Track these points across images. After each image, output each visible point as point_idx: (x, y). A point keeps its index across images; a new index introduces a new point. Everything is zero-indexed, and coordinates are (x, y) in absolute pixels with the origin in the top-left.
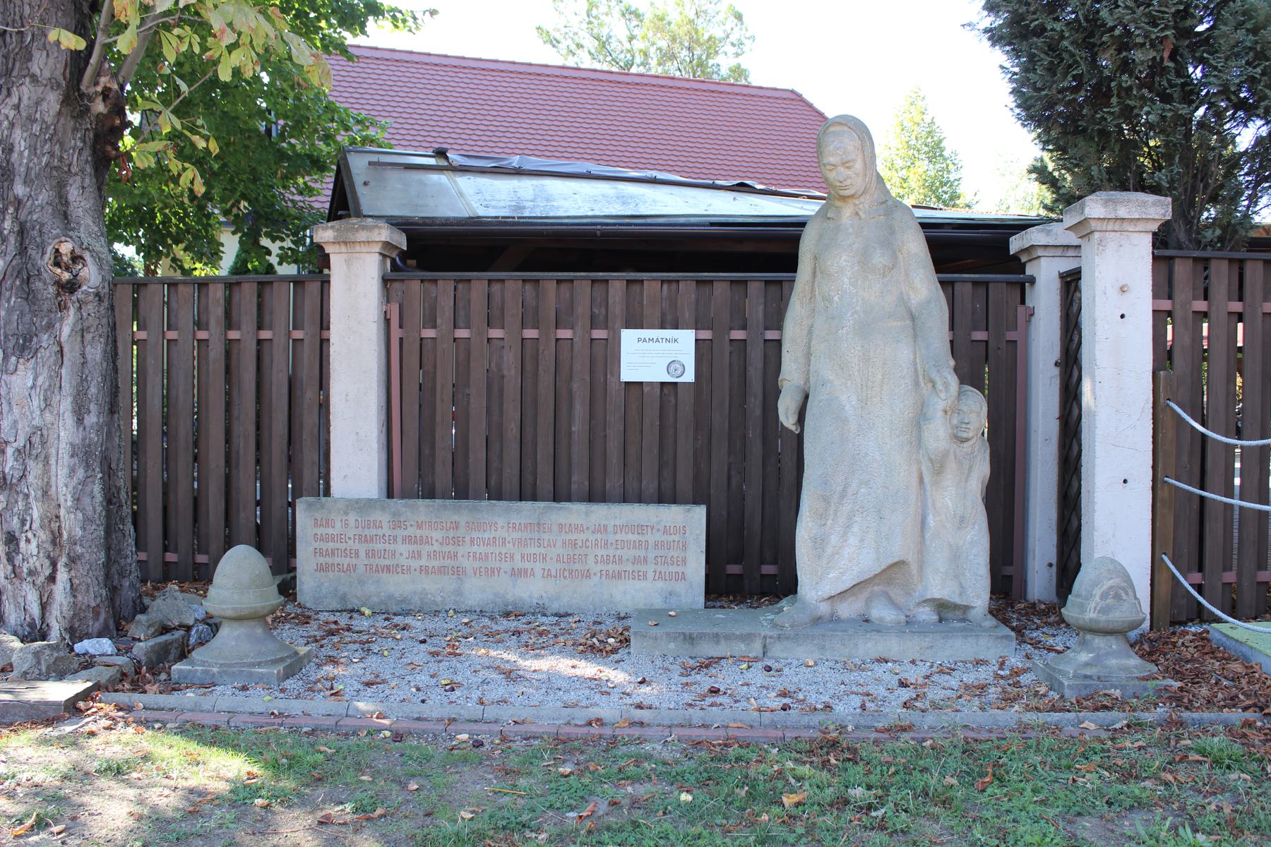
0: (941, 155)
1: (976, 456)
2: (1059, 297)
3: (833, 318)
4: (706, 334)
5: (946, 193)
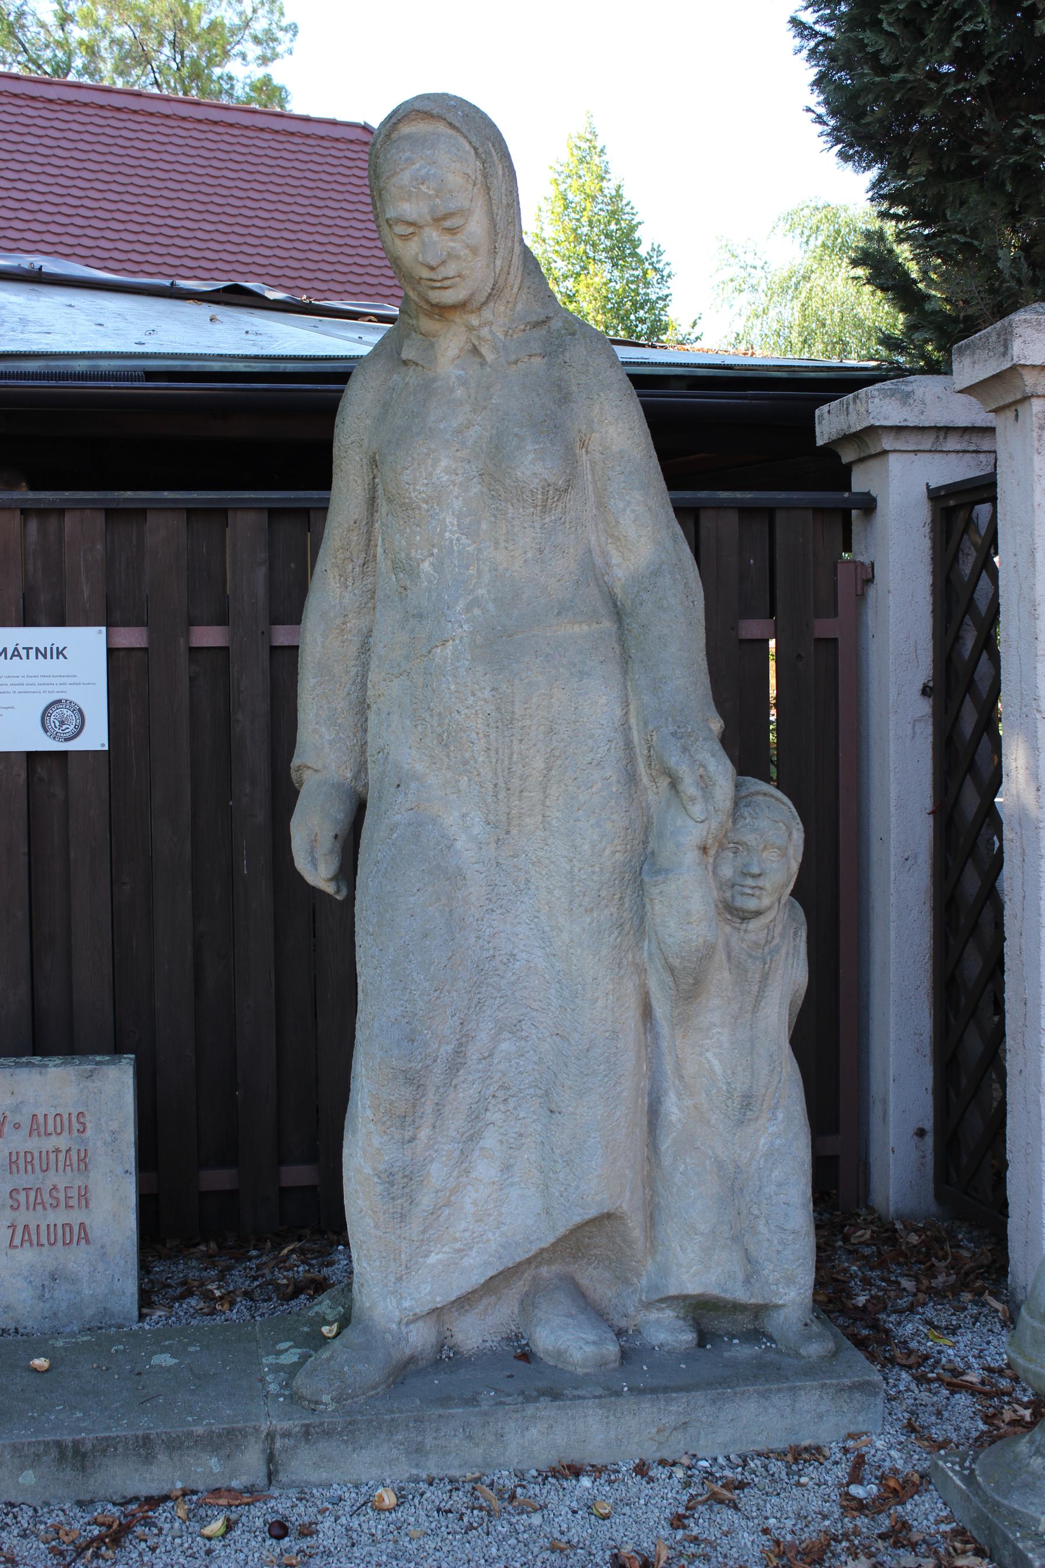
0: (634, 254)
1: (777, 950)
2: (926, 544)
3: (420, 616)
4: (132, 637)
5: (642, 321)
